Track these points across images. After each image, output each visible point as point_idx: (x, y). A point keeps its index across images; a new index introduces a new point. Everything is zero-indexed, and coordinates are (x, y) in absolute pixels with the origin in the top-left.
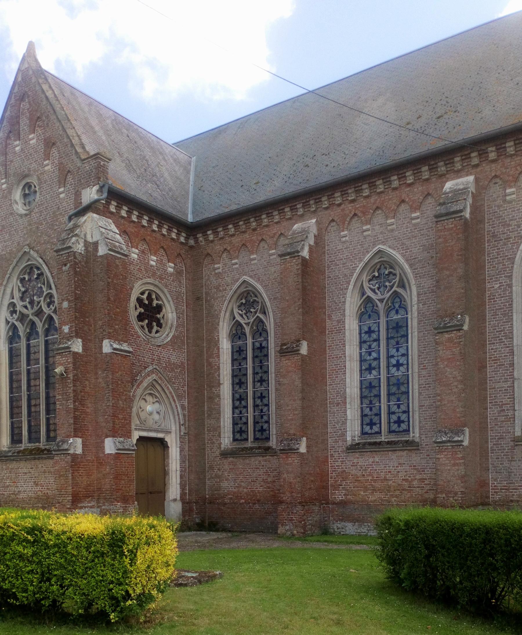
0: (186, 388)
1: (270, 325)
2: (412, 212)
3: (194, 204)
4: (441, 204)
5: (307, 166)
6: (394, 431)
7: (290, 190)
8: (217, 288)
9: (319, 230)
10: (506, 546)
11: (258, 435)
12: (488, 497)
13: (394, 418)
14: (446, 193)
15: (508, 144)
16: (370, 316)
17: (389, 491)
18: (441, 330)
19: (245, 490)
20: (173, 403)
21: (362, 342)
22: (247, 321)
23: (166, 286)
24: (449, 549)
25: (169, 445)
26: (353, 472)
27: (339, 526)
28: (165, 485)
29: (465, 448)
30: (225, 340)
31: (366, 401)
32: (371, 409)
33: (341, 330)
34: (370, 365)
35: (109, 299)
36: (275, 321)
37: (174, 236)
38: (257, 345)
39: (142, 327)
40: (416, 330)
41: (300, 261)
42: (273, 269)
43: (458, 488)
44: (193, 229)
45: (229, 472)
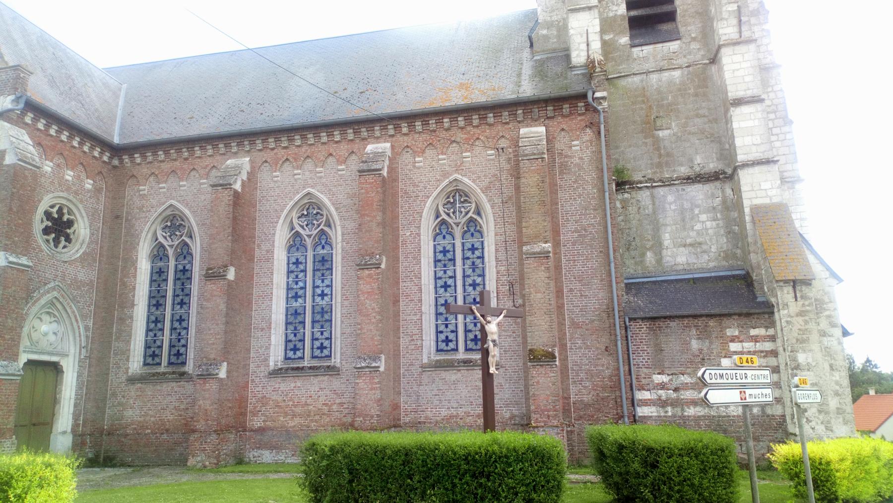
0: (92, 307)
1: (196, 248)
2: (338, 165)
3: (122, 127)
4: (363, 162)
5: (243, 111)
7: (225, 129)
8: (141, 209)
9: (252, 167)
10: (423, 466)
11: (173, 359)
12: (399, 420)
13: (317, 344)
15: (416, 124)
16: (298, 249)
17: (309, 416)
18: (362, 267)
19: (152, 419)
20: (75, 324)
21: (289, 272)
22: (171, 243)
23: (81, 201)
24: (372, 472)
25: (64, 370)
26: (274, 398)
27: (256, 454)
28: (54, 415)
29: (381, 374)
30: (144, 260)
31: (291, 327)
32: (295, 335)
33: (269, 259)
34: (296, 293)
35: (11, 209)
36: (201, 245)
37: (96, 154)
38: (180, 267)
39: (48, 241)
40: (339, 265)
41: (232, 193)
42: (203, 197)
43: (374, 411)
44: (117, 151)
45: (135, 400)
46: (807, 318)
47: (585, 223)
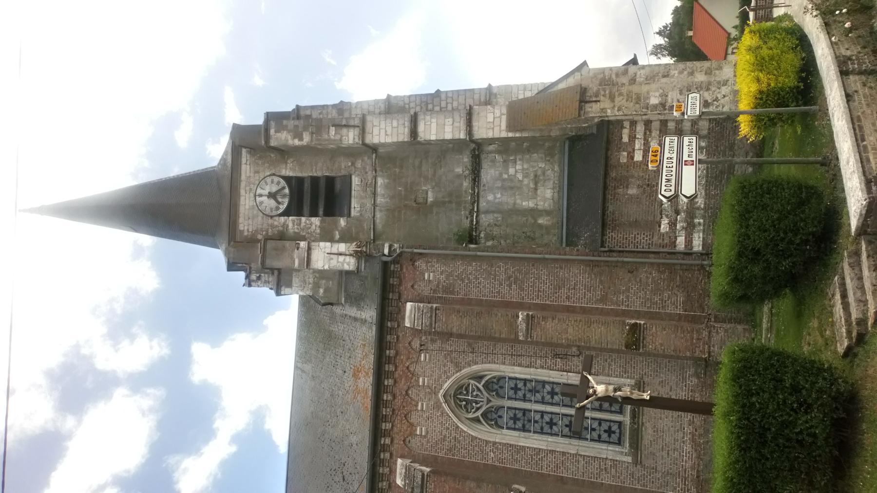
6: (619, 439)
14: (405, 486)
46: (617, 94)
47: (503, 277)
